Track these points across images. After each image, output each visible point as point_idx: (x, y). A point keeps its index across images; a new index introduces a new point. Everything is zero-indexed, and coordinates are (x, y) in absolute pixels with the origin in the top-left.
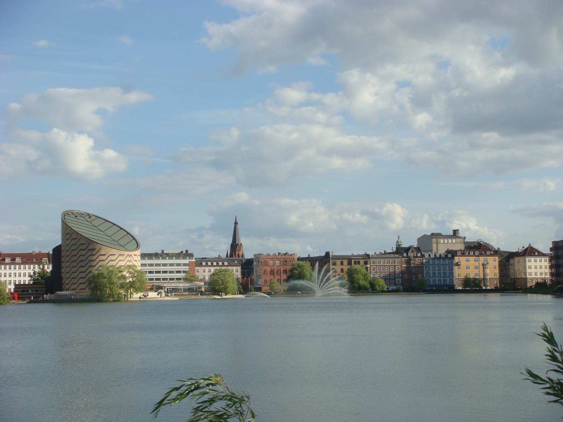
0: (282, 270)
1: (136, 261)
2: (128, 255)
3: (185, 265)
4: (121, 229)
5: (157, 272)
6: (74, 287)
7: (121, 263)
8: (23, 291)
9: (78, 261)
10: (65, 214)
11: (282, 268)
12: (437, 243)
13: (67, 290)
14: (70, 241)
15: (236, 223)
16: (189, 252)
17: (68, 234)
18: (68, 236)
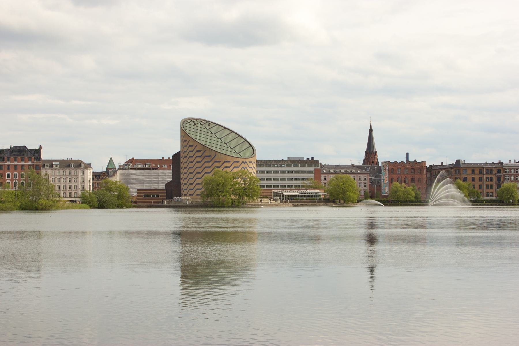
0: (410, 178)
1: (251, 168)
2: (243, 162)
3: (310, 172)
4: (239, 136)
5: (275, 179)
6: (191, 192)
7: (235, 170)
8: (145, 196)
9: (195, 168)
10: (185, 122)
11: (409, 176)
12: (83, 174)
13: (185, 195)
14: (187, 148)
15: (371, 131)
16: (315, 159)
17: (186, 141)
18: (185, 144)
